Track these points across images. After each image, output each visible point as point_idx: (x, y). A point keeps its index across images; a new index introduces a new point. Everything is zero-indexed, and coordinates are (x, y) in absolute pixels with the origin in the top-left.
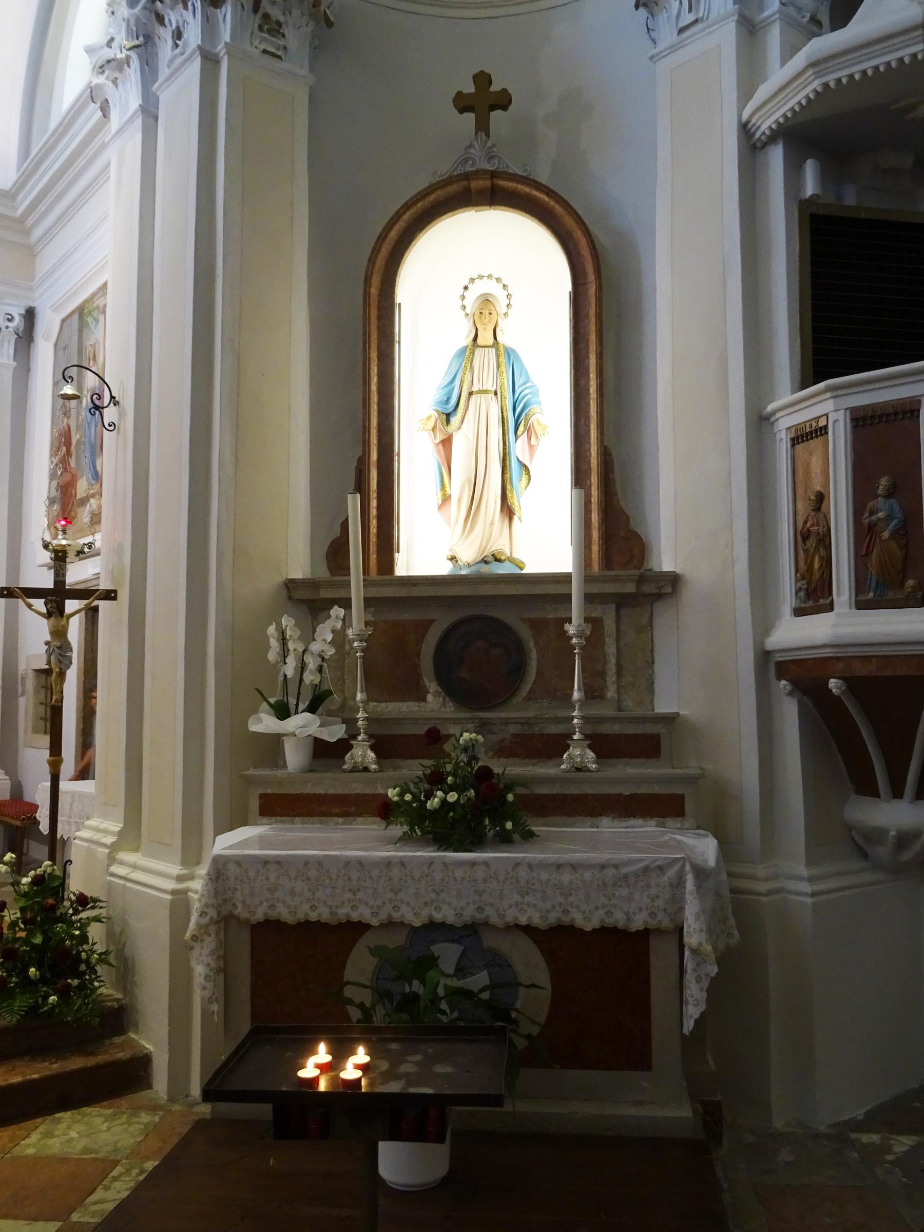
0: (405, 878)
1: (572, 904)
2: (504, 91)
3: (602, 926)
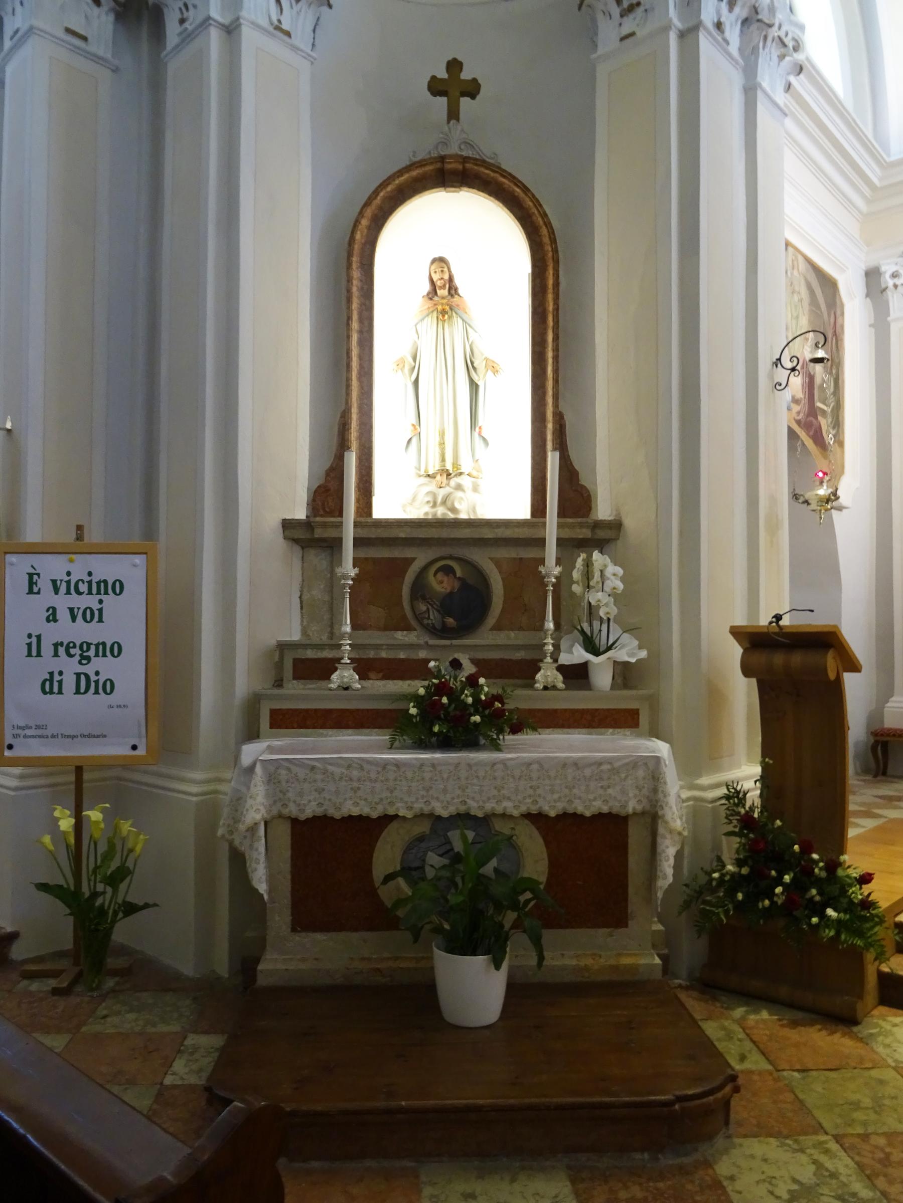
0: (507, 777)
1: (539, 796)
2: (475, 80)
3: (504, 813)
